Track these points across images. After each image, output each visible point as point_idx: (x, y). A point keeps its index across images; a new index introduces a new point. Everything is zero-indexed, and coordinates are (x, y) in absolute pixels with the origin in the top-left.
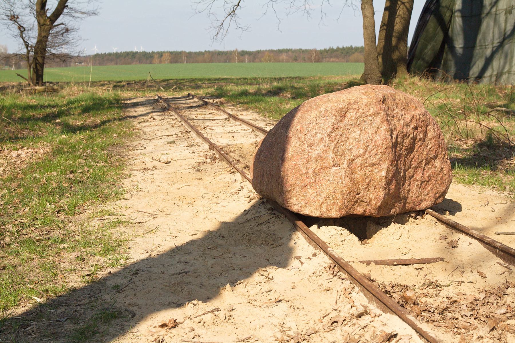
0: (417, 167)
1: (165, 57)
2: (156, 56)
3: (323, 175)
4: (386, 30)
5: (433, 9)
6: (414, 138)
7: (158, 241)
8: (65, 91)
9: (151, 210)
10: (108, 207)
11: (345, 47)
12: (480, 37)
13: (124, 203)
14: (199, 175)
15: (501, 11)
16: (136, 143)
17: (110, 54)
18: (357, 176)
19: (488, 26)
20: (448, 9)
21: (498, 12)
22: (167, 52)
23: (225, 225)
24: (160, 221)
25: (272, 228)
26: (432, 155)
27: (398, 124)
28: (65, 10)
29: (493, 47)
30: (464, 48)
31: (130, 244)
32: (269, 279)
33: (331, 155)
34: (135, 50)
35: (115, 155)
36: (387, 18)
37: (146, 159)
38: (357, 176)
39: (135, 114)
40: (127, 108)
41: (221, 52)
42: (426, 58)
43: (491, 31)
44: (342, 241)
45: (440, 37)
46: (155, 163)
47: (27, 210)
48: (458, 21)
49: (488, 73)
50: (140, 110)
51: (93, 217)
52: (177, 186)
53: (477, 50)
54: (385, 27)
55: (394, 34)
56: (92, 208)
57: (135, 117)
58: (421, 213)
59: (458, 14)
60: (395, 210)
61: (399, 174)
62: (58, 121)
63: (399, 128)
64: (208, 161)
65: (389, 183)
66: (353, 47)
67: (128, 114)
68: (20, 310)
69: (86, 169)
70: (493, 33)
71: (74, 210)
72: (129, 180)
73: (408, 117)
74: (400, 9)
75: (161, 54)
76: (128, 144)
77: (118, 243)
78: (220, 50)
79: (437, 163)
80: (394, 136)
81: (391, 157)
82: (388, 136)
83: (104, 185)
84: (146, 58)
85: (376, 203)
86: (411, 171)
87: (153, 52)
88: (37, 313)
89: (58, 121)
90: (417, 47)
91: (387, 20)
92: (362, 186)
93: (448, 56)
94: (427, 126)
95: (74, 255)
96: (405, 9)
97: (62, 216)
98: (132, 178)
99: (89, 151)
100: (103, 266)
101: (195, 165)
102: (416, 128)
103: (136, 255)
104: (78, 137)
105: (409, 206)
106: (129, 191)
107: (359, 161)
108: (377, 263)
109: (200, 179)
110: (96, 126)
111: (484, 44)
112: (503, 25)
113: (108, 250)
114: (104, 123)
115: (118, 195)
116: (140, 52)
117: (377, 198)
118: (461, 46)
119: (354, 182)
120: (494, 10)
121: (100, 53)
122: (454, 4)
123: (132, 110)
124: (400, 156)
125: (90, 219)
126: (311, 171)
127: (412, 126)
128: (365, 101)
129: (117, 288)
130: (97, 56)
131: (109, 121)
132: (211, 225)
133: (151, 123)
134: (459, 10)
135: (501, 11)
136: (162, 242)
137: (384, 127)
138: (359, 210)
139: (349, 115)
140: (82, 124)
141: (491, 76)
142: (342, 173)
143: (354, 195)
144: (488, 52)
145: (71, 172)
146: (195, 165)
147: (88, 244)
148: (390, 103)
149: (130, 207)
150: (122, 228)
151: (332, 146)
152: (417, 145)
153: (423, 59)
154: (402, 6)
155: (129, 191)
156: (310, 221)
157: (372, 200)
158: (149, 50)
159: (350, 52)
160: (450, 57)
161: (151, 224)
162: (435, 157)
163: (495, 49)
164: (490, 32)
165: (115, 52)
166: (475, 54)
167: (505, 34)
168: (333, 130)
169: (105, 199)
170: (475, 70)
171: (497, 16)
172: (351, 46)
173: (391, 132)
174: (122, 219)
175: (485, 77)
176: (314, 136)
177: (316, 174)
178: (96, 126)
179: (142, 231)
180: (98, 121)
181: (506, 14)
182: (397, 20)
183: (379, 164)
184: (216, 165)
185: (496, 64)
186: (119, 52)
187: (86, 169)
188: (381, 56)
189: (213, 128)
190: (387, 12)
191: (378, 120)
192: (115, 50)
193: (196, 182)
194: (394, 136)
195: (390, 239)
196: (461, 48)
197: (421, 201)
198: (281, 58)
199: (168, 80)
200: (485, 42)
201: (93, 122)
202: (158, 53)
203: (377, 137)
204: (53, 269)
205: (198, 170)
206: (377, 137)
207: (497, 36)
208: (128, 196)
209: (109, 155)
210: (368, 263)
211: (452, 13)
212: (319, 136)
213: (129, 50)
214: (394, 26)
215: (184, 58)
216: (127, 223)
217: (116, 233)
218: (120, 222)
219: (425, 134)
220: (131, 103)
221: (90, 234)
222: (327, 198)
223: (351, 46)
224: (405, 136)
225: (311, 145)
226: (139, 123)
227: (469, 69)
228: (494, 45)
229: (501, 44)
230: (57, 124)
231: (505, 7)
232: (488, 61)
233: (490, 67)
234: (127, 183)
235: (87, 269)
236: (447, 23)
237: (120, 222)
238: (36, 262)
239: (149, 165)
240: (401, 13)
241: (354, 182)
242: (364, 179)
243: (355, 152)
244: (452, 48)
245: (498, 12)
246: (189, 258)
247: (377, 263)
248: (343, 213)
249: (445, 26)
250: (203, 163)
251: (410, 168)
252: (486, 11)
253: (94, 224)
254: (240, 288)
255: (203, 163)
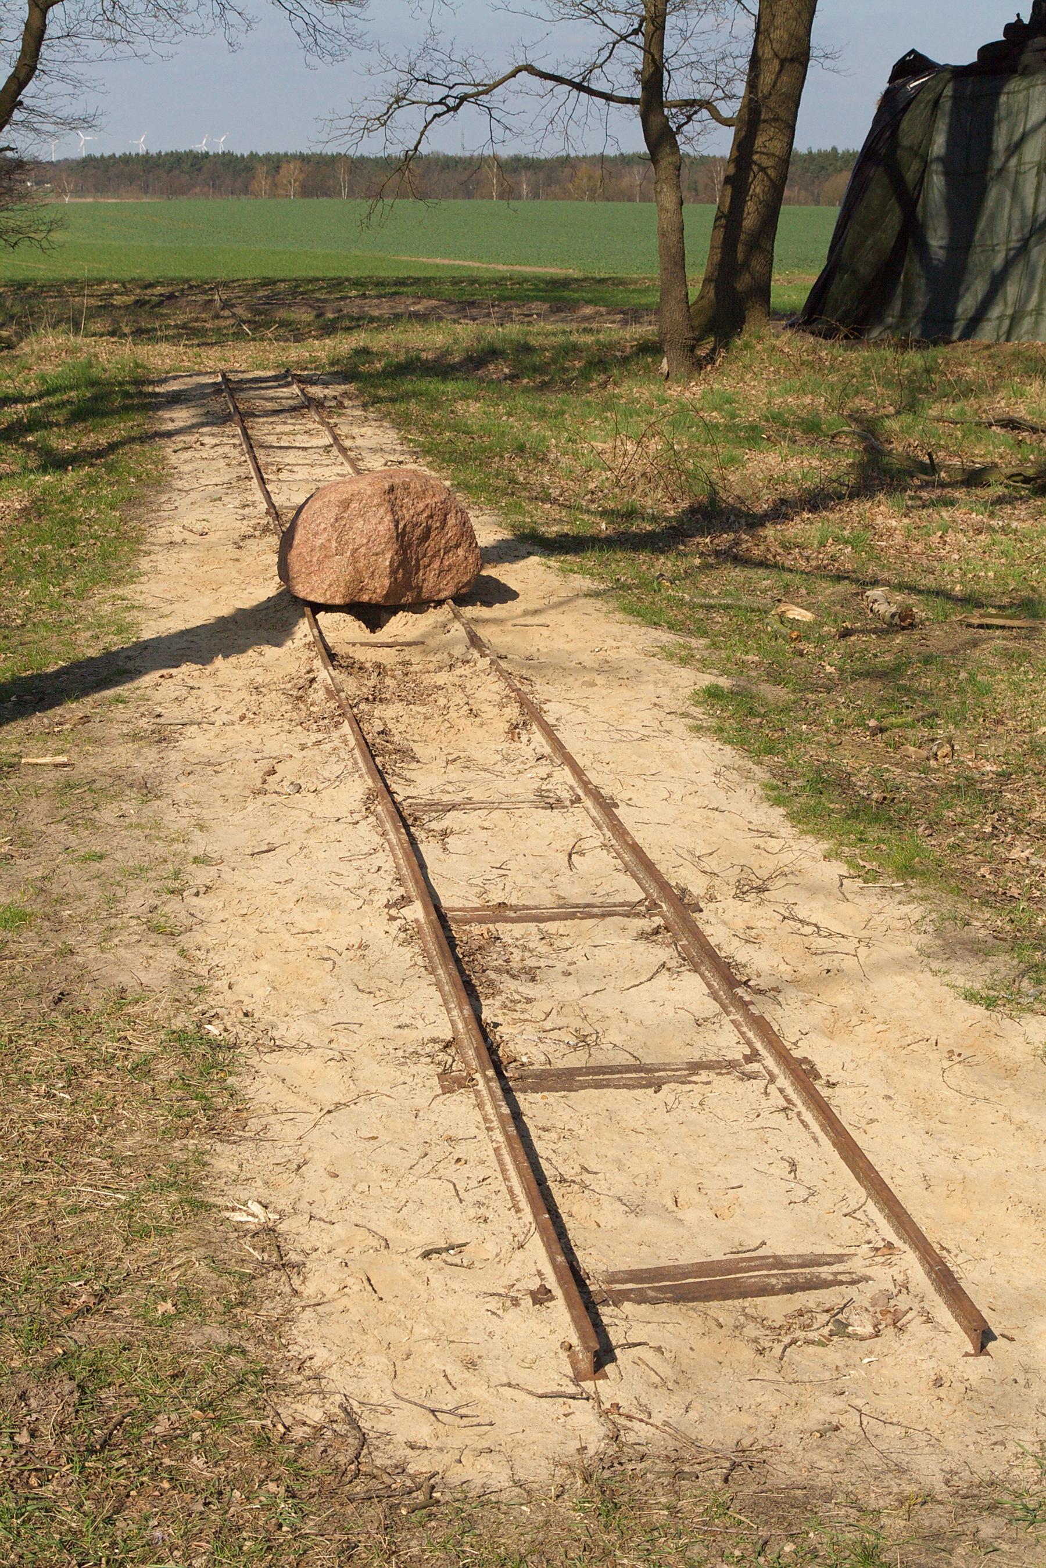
0: (434, 556)
1: (290, 172)
2: (261, 170)
3: (327, 563)
4: (725, 227)
5: (883, 151)
6: (429, 529)
7: (171, 625)
8: (27, 345)
9: (168, 596)
10: (119, 592)
11: (815, 151)
12: (982, 225)
13: (139, 588)
14: (237, 554)
15: (1027, 167)
16: (164, 498)
17: (126, 159)
18: (361, 565)
19: (999, 201)
20: (916, 155)
21: (1022, 169)
22: (294, 157)
23: (241, 611)
24: (176, 606)
25: (286, 615)
26: (452, 543)
27: (407, 515)
28: (17, 115)
29: (1009, 250)
30: (950, 248)
31: (143, 627)
32: (261, 654)
33: (334, 544)
34: (201, 147)
35: (132, 519)
36: (728, 200)
37: (175, 528)
38: (361, 565)
39: (170, 426)
40: (159, 409)
41: (452, 158)
42: (862, 270)
43: (1007, 210)
44: (343, 630)
45: (893, 220)
46: (186, 534)
47: (27, 593)
48: (937, 182)
49: (995, 312)
50: (181, 416)
51: (105, 602)
52: (205, 568)
53: (976, 258)
54: (723, 221)
55: (743, 237)
56: (100, 593)
57: (169, 434)
58: (440, 603)
59: (936, 167)
60: (408, 598)
61: (409, 563)
62: (30, 439)
63: (407, 517)
64: (257, 533)
65: (394, 572)
66: (840, 151)
67: (157, 427)
68: (50, 670)
69: (92, 541)
70: (1010, 218)
71: (82, 594)
72: (147, 559)
73: (421, 506)
74: (756, 182)
75: (275, 163)
76: (152, 498)
77: (131, 625)
78: (451, 153)
79: (461, 552)
80: (401, 526)
81: (396, 546)
82: (392, 526)
83: (116, 565)
84: (230, 173)
85: (381, 591)
86: (426, 560)
87: (253, 156)
88: (63, 671)
89: (30, 439)
90: (841, 248)
91: (727, 204)
92: (366, 575)
93: (912, 266)
94: (446, 515)
95: (89, 634)
96: (767, 183)
97: (70, 601)
98: (153, 557)
99: (93, 512)
100: (115, 642)
101: (238, 540)
102: (431, 516)
103: (147, 635)
104: (70, 479)
105: (425, 595)
106: (146, 574)
107: (363, 550)
108: (362, 644)
109: (237, 560)
110: (99, 454)
111: (989, 242)
112: (1030, 202)
113: (119, 632)
114: (112, 447)
115: (132, 579)
116: (216, 155)
117: (383, 586)
118: (943, 243)
119: (357, 571)
120: (1013, 162)
121: (98, 155)
122: (930, 142)
123: (167, 415)
124: (410, 545)
125: (103, 602)
126: (315, 559)
127: (425, 515)
128: (369, 492)
129: (129, 658)
130: (89, 161)
131: (122, 443)
132: (225, 611)
133: (195, 454)
134: (938, 159)
135: (1027, 167)
136: (175, 625)
137: (389, 517)
138: (365, 598)
139: (352, 506)
140: (75, 448)
141: (1000, 318)
142: (345, 562)
143: (357, 583)
144: (998, 262)
145: (72, 546)
146: (238, 540)
147: (100, 626)
148: (399, 493)
149: (148, 591)
150: (136, 613)
151: (335, 536)
152: (433, 534)
153: (854, 272)
154: (760, 175)
155: (146, 574)
156: (317, 608)
157: (377, 588)
158: (241, 149)
159: (831, 168)
160: (917, 269)
161: (167, 609)
162: (457, 546)
163: (1012, 253)
164: (1002, 221)
165: (142, 151)
166: (971, 265)
167: (1035, 220)
168: (337, 520)
169: (118, 582)
170: (967, 305)
171: (1021, 178)
172: (834, 149)
173: (397, 523)
174: (136, 604)
175: (989, 320)
176: (318, 525)
177: (320, 562)
178: (99, 454)
179: (155, 616)
180: (103, 441)
181: (1038, 173)
182: (750, 207)
183: (383, 553)
184: (266, 539)
185: (1012, 290)
186: (153, 151)
187: (92, 541)
188: (713, 285)
189: (295, 469)
190: (729, 190)
191: (382, 510)
192: (141, 145)
193: (230, 564)
194: (401, 526)
195: (401, 626)
196: (941, 247)
197: (440, 591)
198: (626, 182)
199: (274, 282)
200: (992, 238)
201: (93, 444)
202: (268, 157)
203: (381, 528)
204: (72, 644)
205: (240, 547)
206: (381, 528)
207: (1016, 224)
208: (144, 579)
209: (123, 521)
210: (354, 645)
211: (926, 165)
212: (323, 526)
213: (182, 147)
214: (742, 220)
215: (343, 176)
216: (141, 608)
217: (129, 617)
218: (133, 607)
219: (444, 522)
220: (167, 394)
221: (102, 617)
222: (330, 585)
223: (834, 149)
224: (416, 525)
225: (315, 535)
226: (175, 452)
227: (957, 298)
228: (1012, 245)
229: (1023, 249)
230: (29, 447)
231: (1037, 158)
232: (998, 282)
233: (999, 298)
234: (144, 564)
235: (102, 645)
236: (911, 188)
237: (133, 607)
238: (55, 639)
239: (177, 538)
240: (758, 190)
241: (357, 571)
242: (368, 568)
243: (358, 541)
244: (923, 247)
245: (1022, 169)
246: (195, 638)
247: (362, 644)
248: (348, 600)
249: (908, 199)
250: (250, 537)
251: (425, 556)
252: (997, 164)
253: (107, 608)
254: (233, 659)
255: (250, 537)
